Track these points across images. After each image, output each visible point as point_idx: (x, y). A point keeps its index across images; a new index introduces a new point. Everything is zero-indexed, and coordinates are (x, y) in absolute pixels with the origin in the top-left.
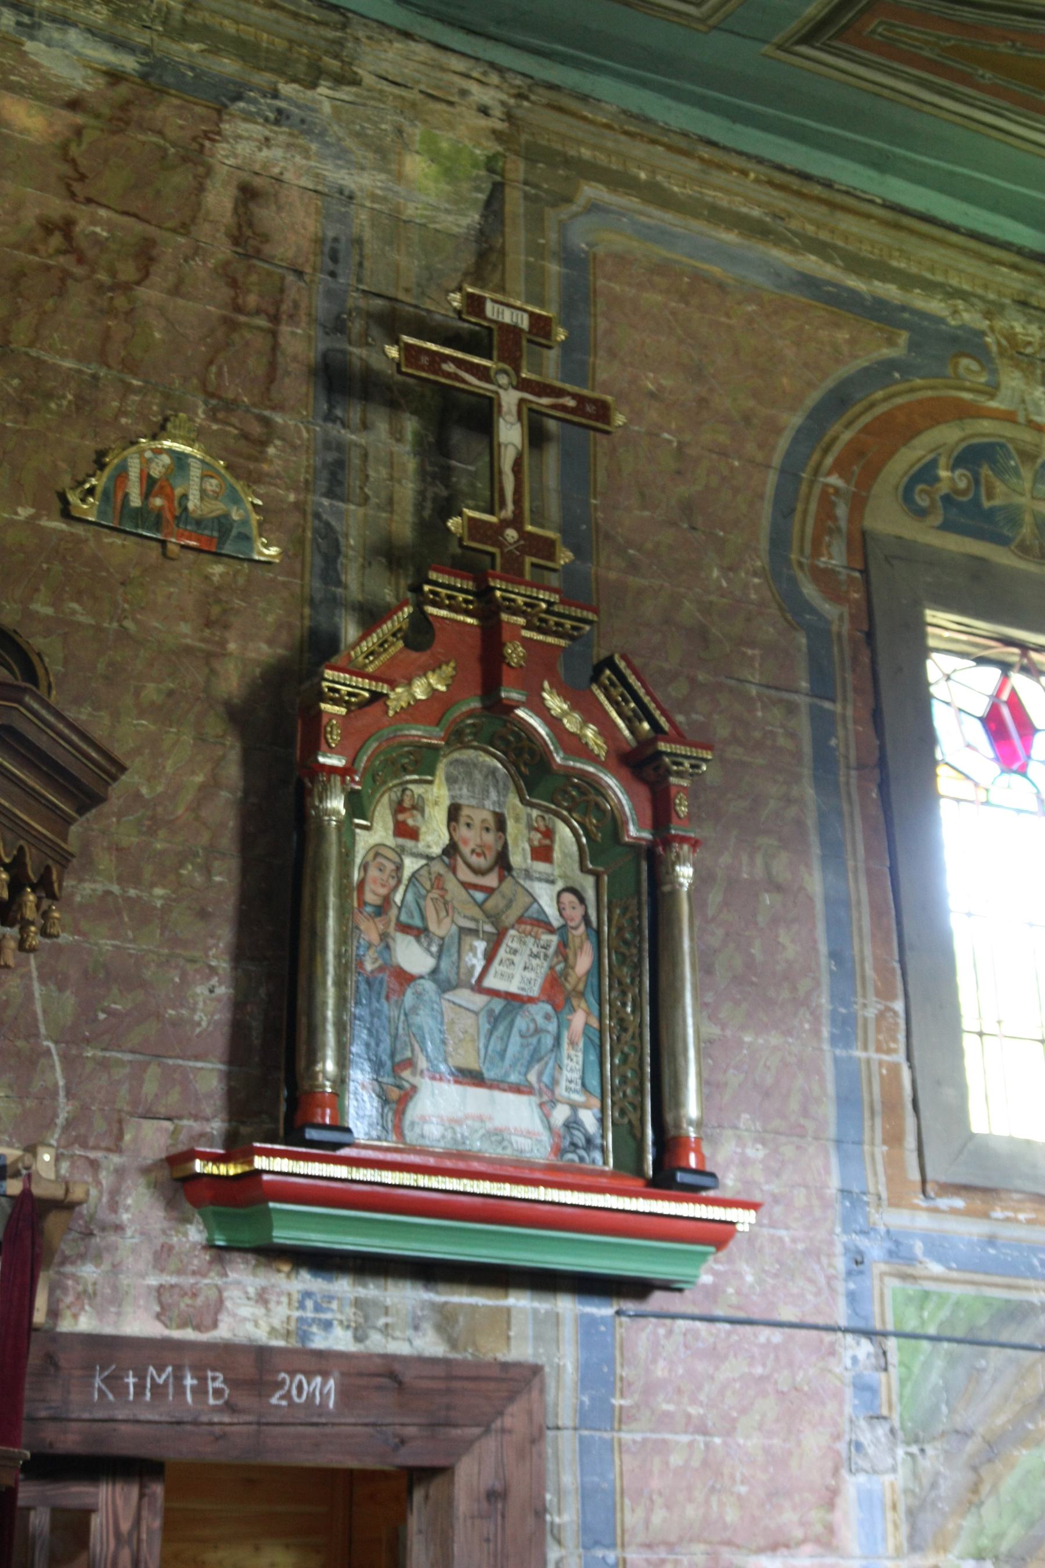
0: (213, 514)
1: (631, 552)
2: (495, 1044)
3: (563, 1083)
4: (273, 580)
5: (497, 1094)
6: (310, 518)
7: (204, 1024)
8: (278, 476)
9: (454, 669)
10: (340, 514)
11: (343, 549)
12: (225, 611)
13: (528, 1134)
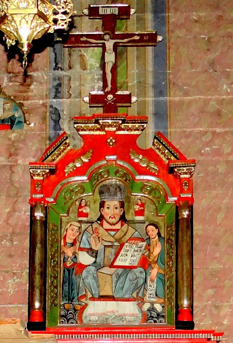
0: (8, 117)
1: (185, 88)
2: (119, 285)
3: (148, 295)
4: (34, 134)
5: (120, 302)
6: (48, 107)
7: (12, 292)
8: (35, 96)
9: (92, 153)
10: (60, 104)
11: (62, 116)
12: (16, 149)
13: (133, 315)
